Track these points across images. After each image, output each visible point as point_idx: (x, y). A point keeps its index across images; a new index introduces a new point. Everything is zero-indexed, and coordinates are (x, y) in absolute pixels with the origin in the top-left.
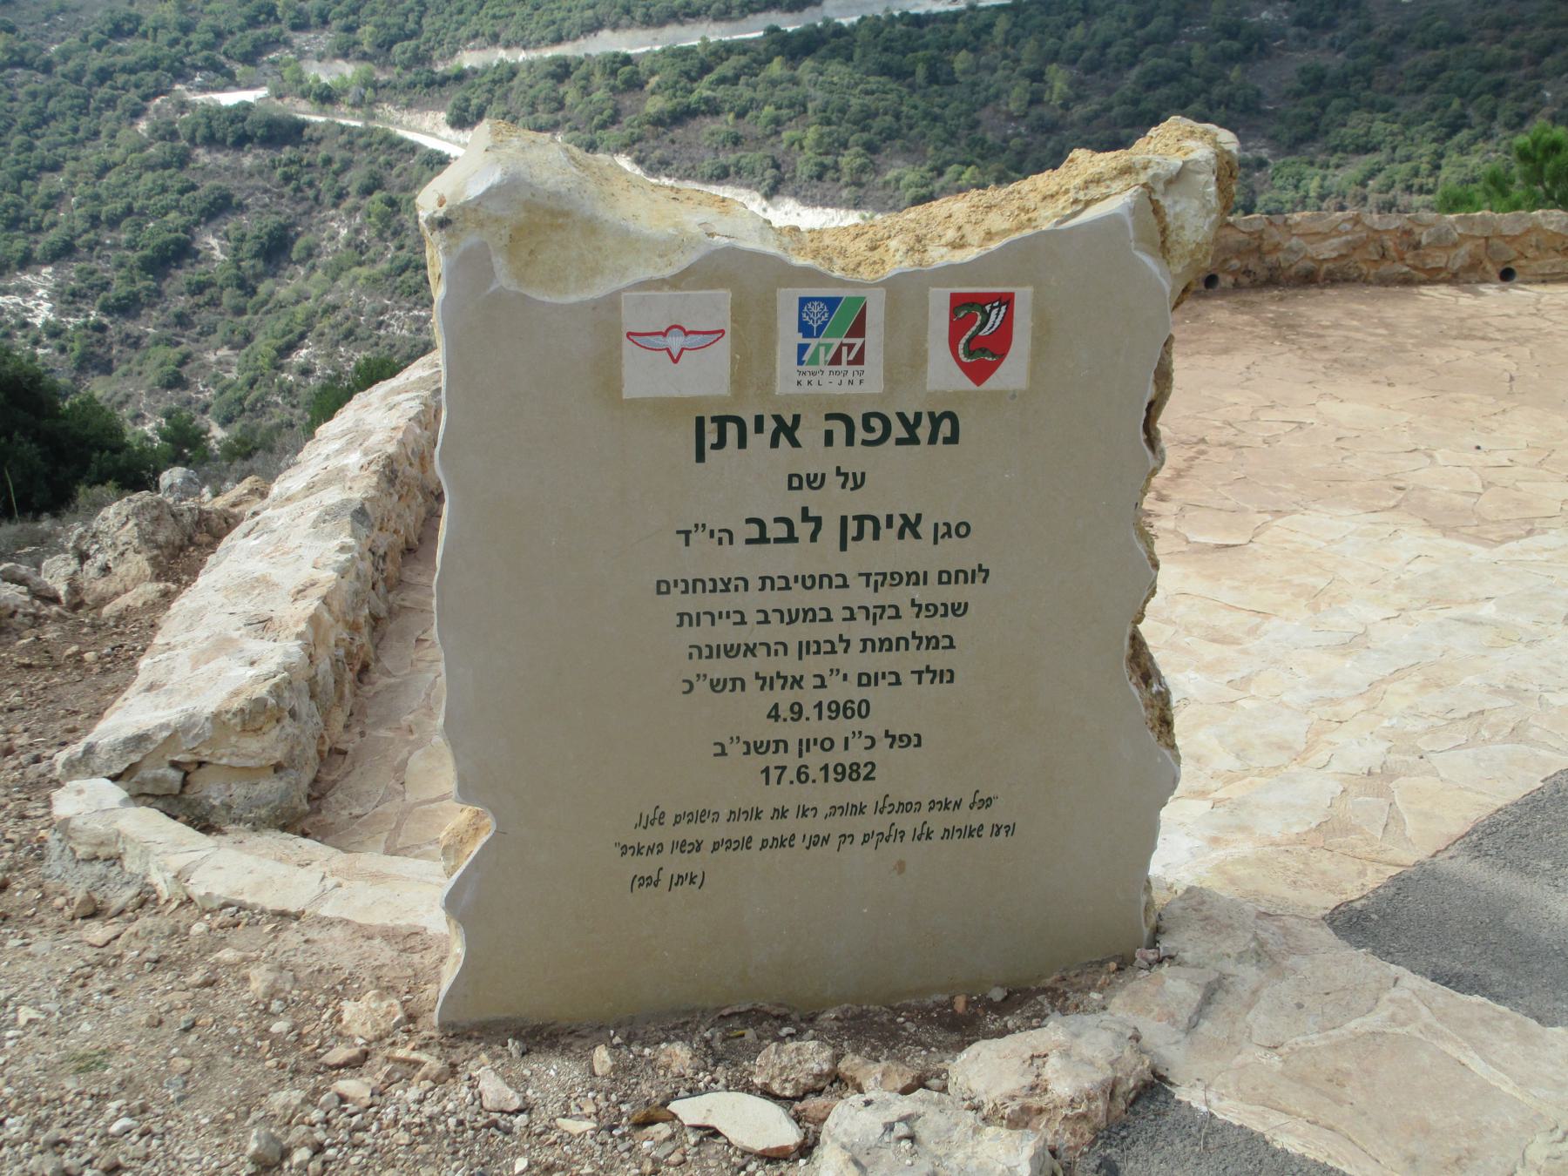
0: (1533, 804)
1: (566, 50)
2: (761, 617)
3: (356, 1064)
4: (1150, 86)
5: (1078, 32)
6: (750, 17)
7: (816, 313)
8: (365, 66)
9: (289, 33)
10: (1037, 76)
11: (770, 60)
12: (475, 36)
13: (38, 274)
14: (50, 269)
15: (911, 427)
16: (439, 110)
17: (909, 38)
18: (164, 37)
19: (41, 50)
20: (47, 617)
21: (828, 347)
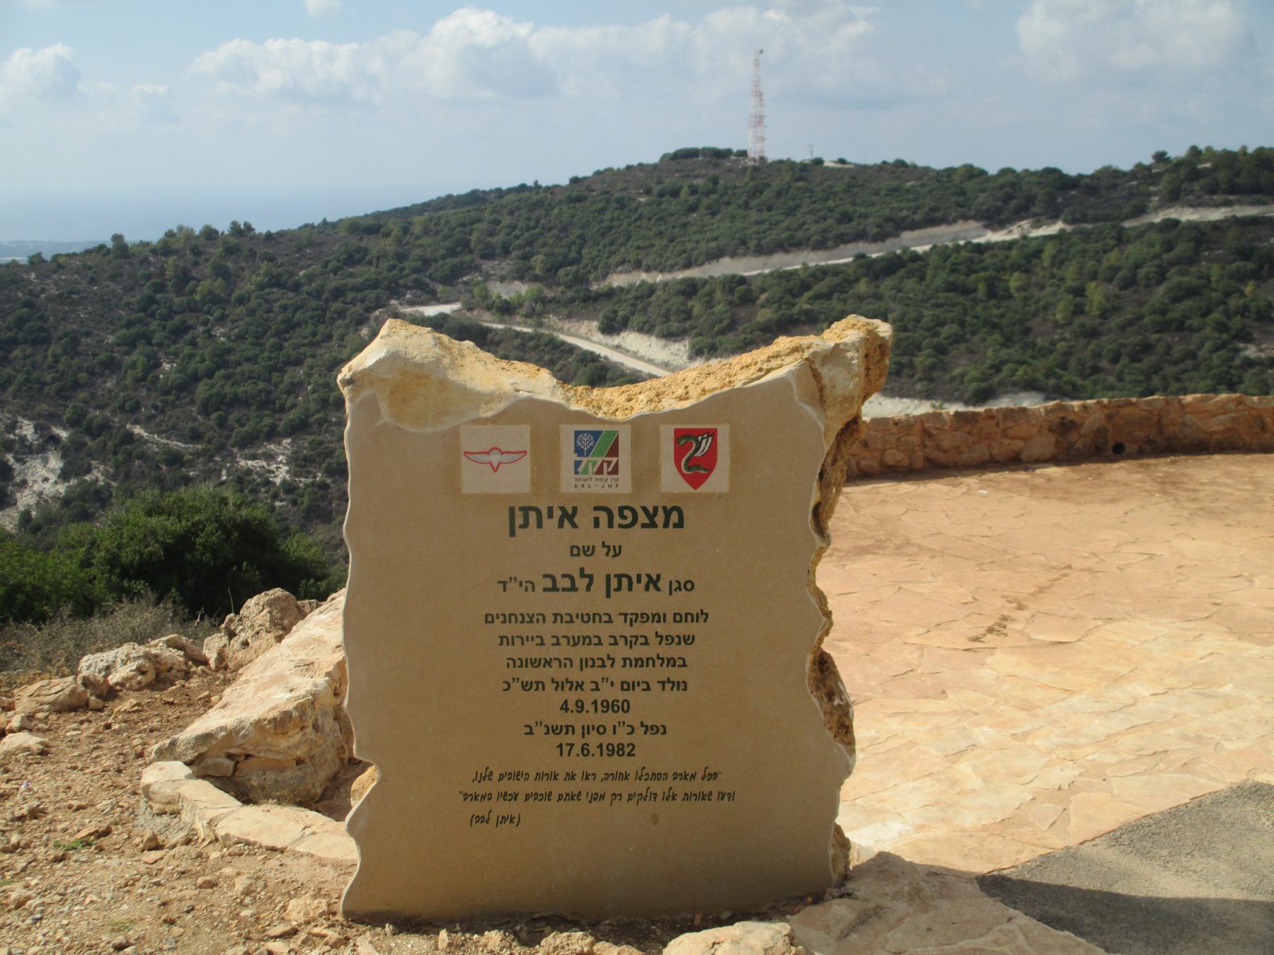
0: (1175, 813)
1: (694, 273)
2: (554, 641)
3: (286, 936)
4: (1176, 300)
5: (1112, 257)
6: (842, 246)
7: (586, 442)
8: (537, 286)
9: (479, 261)
10: (1079, 292)
11: (857, 280)
12: (623, 262)
13: (279, 444)
14: (289, 440)
15: (651, 516)
16: (592, 319)
17: (972, 261)
18: (384, 264)
19: (292, 274)
20: (195, 673)
21: (594, 463)
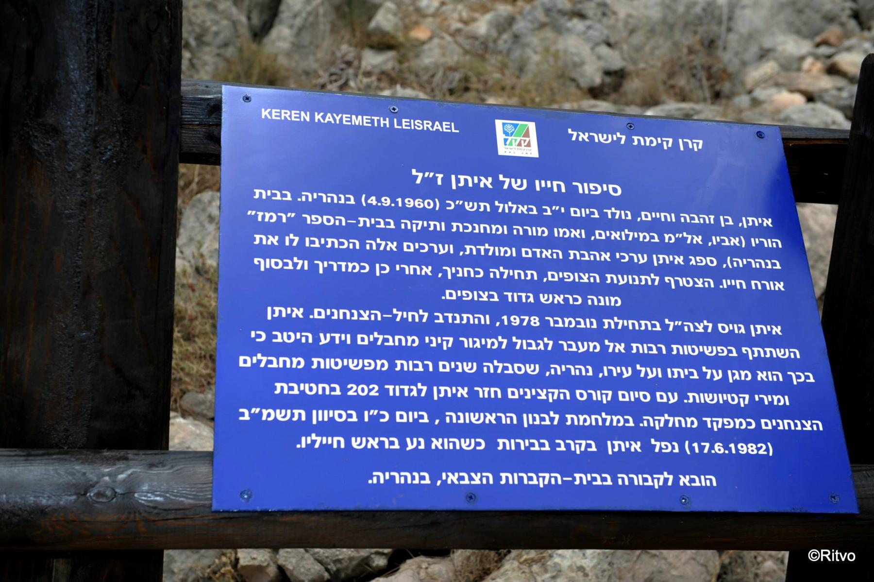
21: (516, 140)
